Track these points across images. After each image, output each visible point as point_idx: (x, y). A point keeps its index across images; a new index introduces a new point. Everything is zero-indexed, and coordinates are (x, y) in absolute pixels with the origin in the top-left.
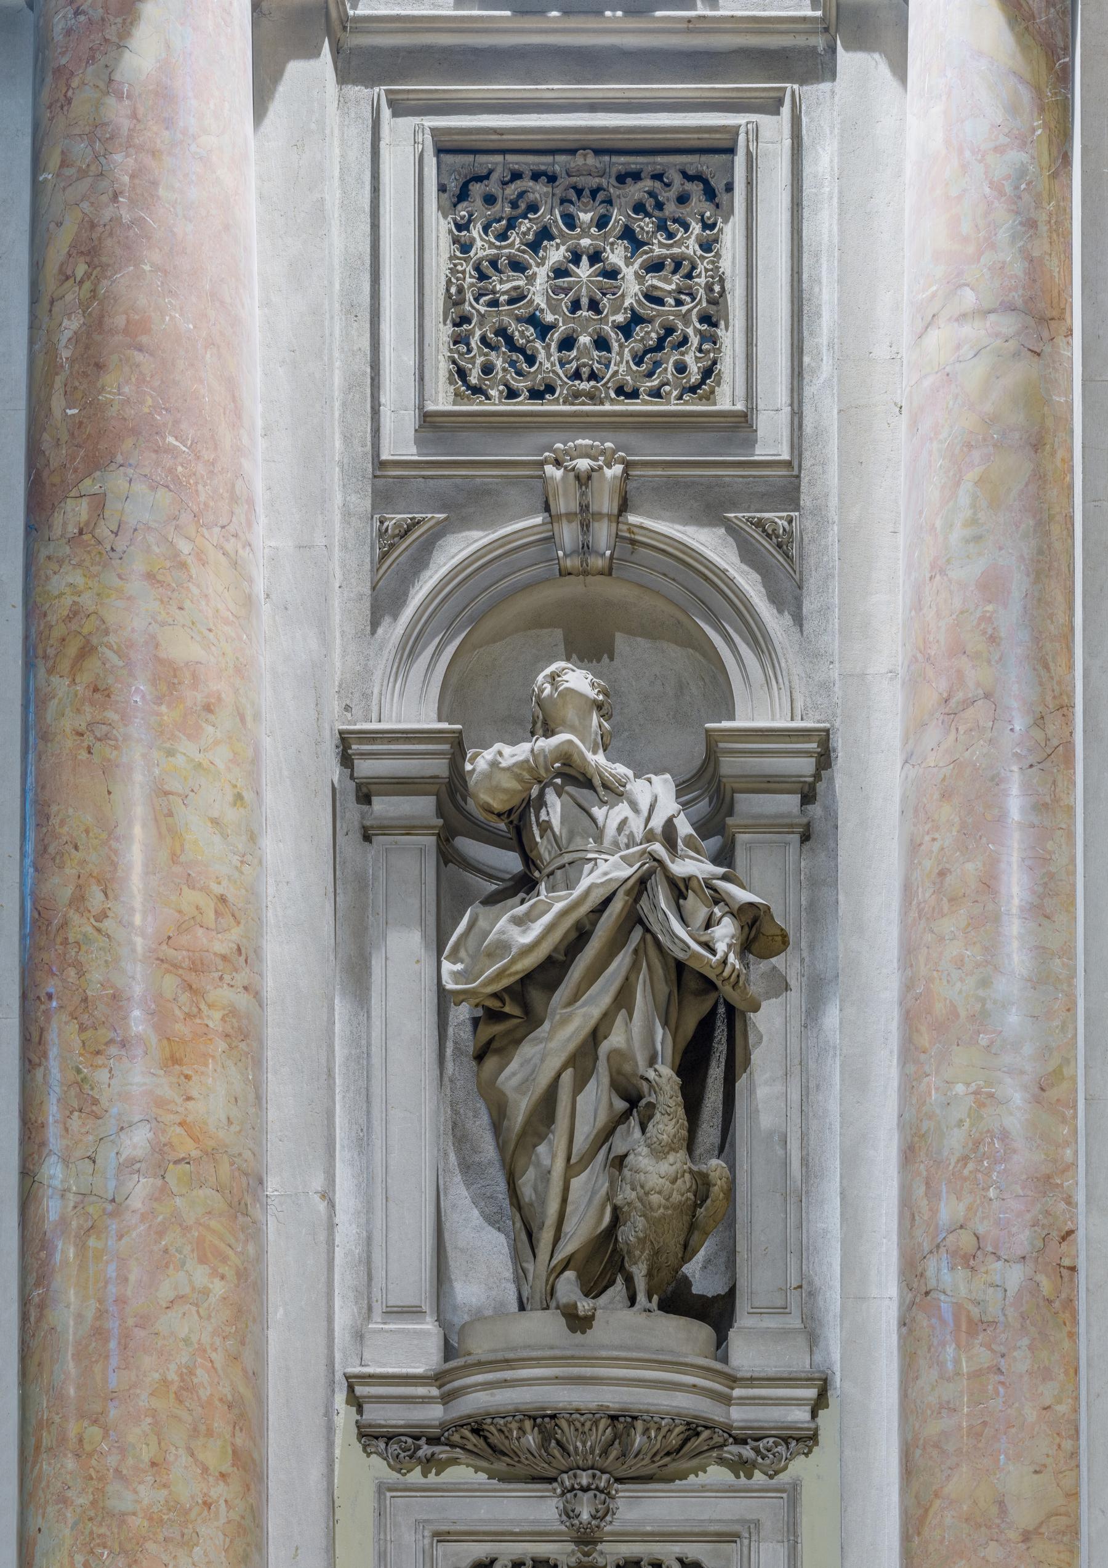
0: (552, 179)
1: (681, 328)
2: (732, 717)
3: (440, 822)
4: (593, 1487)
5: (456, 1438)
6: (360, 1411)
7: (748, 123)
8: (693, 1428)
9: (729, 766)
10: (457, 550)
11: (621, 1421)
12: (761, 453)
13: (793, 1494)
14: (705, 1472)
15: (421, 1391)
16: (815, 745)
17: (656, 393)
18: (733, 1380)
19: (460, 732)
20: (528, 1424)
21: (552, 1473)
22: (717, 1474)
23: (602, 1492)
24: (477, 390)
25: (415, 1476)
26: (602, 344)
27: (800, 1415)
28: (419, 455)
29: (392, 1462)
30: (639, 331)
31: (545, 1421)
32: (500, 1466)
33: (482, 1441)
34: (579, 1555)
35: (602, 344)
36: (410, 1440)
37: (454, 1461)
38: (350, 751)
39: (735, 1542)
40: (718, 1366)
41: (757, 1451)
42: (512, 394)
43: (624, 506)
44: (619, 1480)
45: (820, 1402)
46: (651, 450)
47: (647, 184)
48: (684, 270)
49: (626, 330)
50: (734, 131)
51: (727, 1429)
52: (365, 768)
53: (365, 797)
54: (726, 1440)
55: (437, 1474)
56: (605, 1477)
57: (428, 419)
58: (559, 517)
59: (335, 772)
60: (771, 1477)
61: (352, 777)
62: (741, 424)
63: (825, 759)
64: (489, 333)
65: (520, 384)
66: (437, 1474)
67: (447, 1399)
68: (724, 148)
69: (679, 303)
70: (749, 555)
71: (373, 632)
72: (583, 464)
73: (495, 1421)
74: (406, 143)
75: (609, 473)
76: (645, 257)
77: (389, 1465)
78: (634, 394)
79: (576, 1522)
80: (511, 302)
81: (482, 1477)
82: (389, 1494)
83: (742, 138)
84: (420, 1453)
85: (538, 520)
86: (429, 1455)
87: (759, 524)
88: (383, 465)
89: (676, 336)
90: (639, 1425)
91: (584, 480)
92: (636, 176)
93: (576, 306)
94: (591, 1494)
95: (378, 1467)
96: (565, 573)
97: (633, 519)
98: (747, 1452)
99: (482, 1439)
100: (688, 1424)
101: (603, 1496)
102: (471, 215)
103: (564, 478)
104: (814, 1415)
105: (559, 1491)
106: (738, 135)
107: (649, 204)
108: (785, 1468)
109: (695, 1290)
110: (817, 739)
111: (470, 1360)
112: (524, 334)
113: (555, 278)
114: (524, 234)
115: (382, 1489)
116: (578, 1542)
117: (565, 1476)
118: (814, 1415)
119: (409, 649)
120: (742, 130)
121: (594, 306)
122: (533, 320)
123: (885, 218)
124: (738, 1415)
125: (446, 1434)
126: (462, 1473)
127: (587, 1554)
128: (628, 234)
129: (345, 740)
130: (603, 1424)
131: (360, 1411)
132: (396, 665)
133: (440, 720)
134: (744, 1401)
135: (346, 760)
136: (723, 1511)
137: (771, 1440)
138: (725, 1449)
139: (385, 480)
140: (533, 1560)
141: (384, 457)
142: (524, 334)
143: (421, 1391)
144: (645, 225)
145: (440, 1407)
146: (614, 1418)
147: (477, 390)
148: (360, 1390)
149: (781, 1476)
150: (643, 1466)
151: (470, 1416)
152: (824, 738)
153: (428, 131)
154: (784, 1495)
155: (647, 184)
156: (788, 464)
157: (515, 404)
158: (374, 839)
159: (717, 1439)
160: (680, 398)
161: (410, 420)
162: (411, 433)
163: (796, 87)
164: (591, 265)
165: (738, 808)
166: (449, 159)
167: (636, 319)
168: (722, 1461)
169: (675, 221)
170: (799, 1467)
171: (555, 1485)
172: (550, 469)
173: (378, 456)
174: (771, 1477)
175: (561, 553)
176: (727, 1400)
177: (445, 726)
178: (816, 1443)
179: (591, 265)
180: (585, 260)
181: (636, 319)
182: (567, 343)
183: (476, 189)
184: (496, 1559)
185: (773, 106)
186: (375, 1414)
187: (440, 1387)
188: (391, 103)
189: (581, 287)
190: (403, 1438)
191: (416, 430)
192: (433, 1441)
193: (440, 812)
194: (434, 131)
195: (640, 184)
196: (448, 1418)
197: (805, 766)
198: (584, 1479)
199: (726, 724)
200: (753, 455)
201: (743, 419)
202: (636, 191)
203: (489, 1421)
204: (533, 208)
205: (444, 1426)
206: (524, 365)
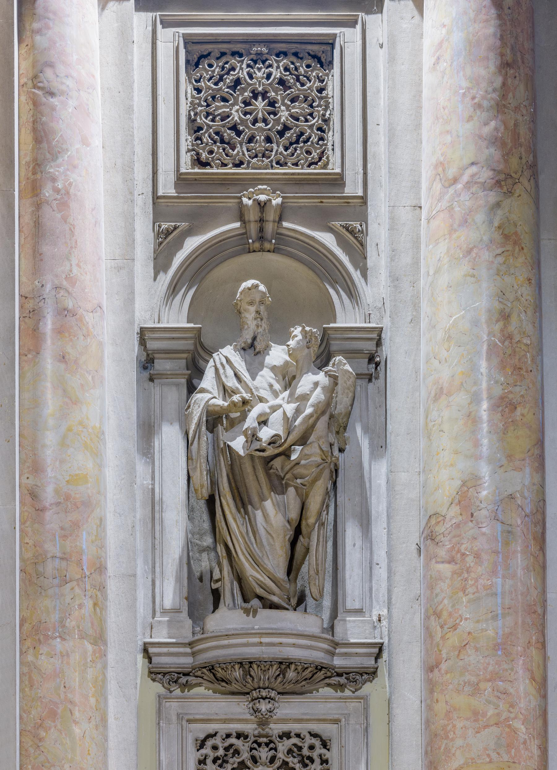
1: (305, 137)
2: (335, 322)
7: (341, 32)
8: (319, 668)
10: (192, 243)
11: (285, 664)
13: (365, 699)
15: (181, 650)
16: (376, 335)
17: (296, 164)
18: (337, 645)
19: (201, 328)
20: (237, 667)
21: (247, 690)
22: (328, 691)
30: (287, 135)
31: (247, 665)
32: (217, 686)
33: (212, 675)
35: (268, 140)
36: (176, 675)
37: (199, 685)
41: (347, 679)
42: (224, 165)
44: (279, 693)
45: (378, 656)
49: (281, 133)
50: (335, 35)
52: (152, 345)
55: (188, 691)
56: (274, 692)
60: (354, 692)
62: (338, 181)
63: (379, 343)
64: (211, 135)
65: (227, 160)
66: (188, 691)
67: (194, 654)
68: (329, 43)
70: (342, 242)
71: (155, 279)
73: (221, 665)
74: (169, 40)
77: (163, 686)
82: (164, 701)
83: (338, 39)
88: (158, 198)
93: (255, 121)
95: (158, 688)
97: (285, 224)
98: (342, 680)
99: (214, 674)
101: (273, 701)
104: (376, 662)
105: (250, 699)
106: (336, 37)
108: (361, 688)
111: (209, 635)
112: (228, 134)
113: (245, 107)
117: (254, 692)
118: (376, 662)
119: (173, 289)
120: (338, 35)
121: (265, 121)
122: (234, 128)
124: (338, 662)
125: (194, 671)
127: (263, 730)
129: (143, 331)
130: (275, 667)
133: (188, 322)
135: (142, 342)
137: (354, 674)
138: (332, 679)
142: (228, 134)
143: (181, 650)
146: (281, 663)
148: (151, 650)
149: (359, 691)
150: (289, 687)
151: (209, 663)
153: (181, 35)
154: (362, 701)
156: (362, 198)
157: (227, 169)
158: (155, 381)
159: (329, 674)
161: (172, 178)
163: (363, 14)
164: (263, 100)
167: (286, 128)
170: (367, 688)
173: (179, 171)
174: (354, 692)
175: (250, 241)
177: (192, 325)
179: (263, 100)
180: (260, 98)
181: (286, 128)
182: (251, 140)
185: (352, 24)
187: (191, 648)
188: (162, 22)
189: (258, 112)
190: (173, 674)
192: (186, 674)
197: (370, 346)
198: (264, 693)
199: (332, 325)
200: (343, 193)
203: (218, 665)
206: (230, 150)
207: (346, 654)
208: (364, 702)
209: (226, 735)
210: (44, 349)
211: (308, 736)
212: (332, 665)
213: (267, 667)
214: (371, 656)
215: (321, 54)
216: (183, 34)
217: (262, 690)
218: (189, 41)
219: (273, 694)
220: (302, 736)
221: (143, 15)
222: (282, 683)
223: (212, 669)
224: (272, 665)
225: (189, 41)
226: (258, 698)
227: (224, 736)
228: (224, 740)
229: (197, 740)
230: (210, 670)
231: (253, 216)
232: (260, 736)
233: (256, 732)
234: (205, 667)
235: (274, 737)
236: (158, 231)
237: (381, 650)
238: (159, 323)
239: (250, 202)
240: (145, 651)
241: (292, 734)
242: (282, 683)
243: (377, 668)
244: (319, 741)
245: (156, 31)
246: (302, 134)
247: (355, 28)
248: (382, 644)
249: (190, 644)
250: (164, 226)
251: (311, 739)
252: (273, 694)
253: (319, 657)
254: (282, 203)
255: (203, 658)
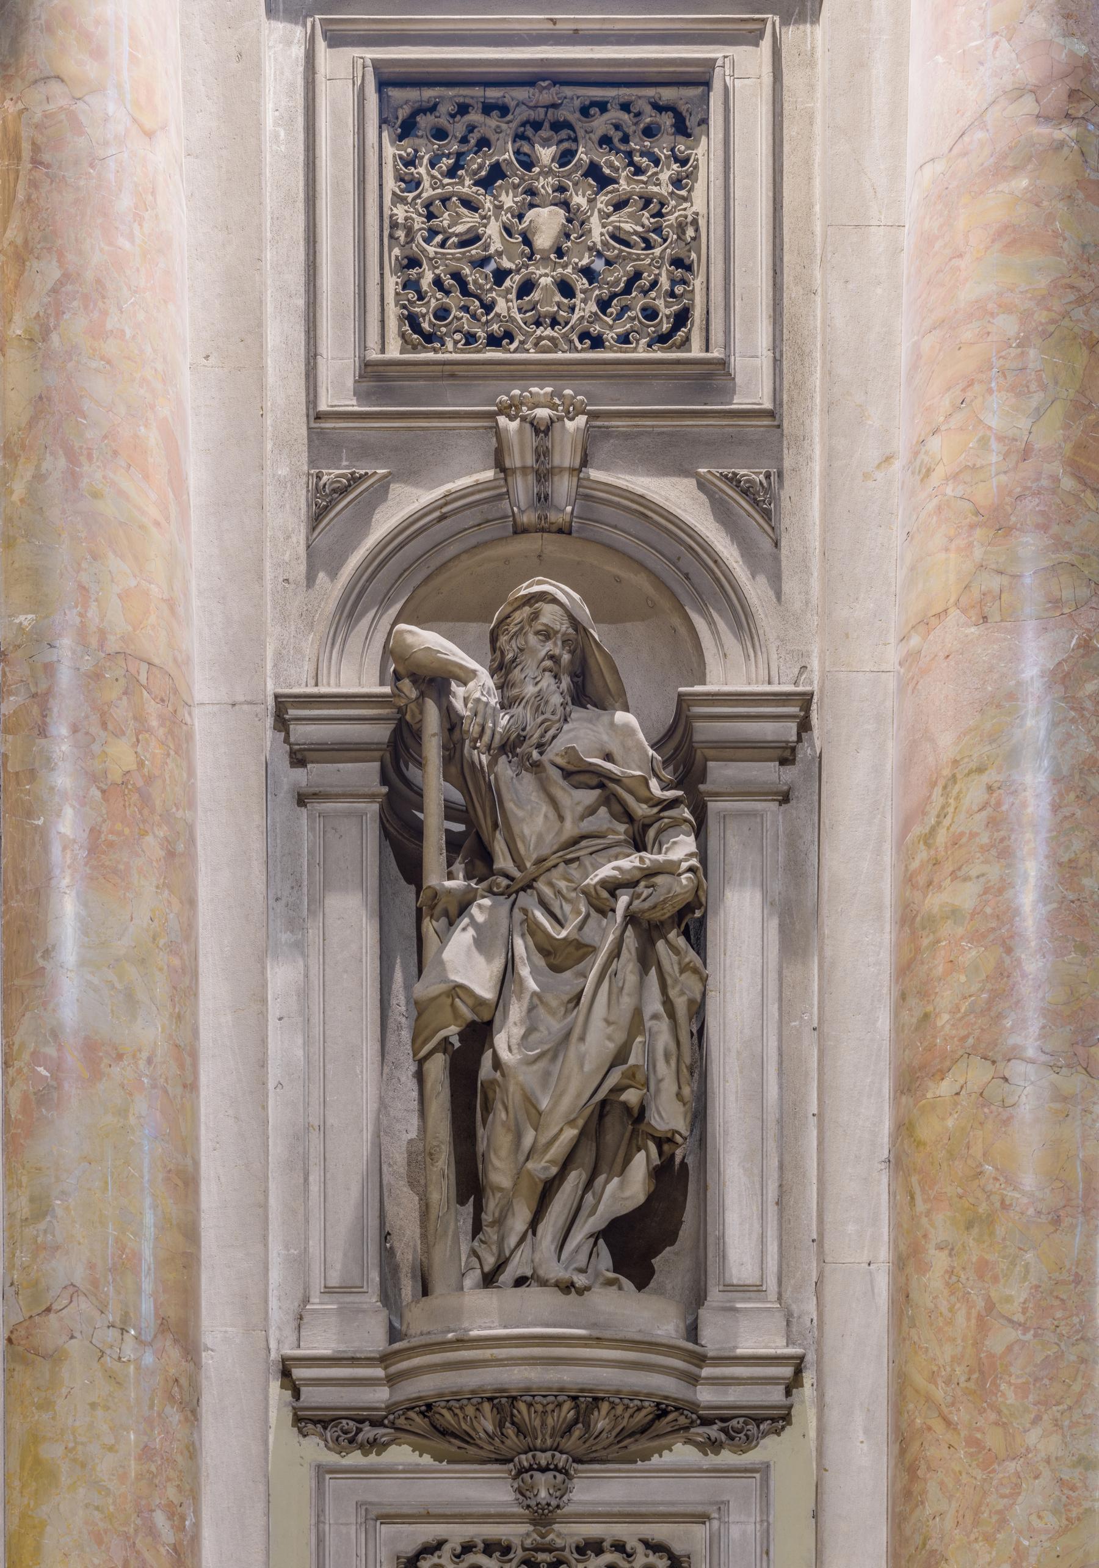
0: (504, 110)
3: (385, 790)
4: (552, 1467)
5: (401, 1422)
6: (297, 1394)
8: (661, 1412)
9: (704, 731)
10: (408, 502)
11: (585, 1403)
12: (739, 402)
14: (671, 1450)
16: (797, 709)
18: (701, 1359)
20: (487, 1407)
23: (560, 1472)
24: (429, 338)
25: (356, 1458)
26: (566, 288)
27: (775, 1395)
28: (359, 406)
29: (331, 1444)
31: (504, 1403)
32: (441, 1445)
34: (535, 1536)
38: (287, 717)
39: (704, 1523)
40: (690, 1346)
41: (723, 1430)
43: (584, 463)
44: (578, 1461)
46: (615, 402)
47: (615, 114)
48: (654, 207)
50: (711, 63)
51: (694, 1407)
52: (302, 733)
53: (299, 758)
54: (692, 1422)
57: (369, 369)
58: (514, 471)
59: (268, 734)
61: (286, 740)
62: (713, 376)
63: (805, 726)
67: (391, 1380)
68: (700, 79)
69: (649, 246)
70: (723, 513)
72: (543, 413)
74: (343, 71)
75: (570, 425)
76: (610, 196)
78: (597, 343)
79: (533, 1503)
80: (463, 244)
81: (427, 1460)
82: (328, 1476)
84: (360, 1437)
85: (490, 474)
86: (371, 1439)
87: (733, 480)
88: (319, 417)
89: (645, 282)
90: (605, 1407)
91: (542, 430)
92: (603, 107)
94: (550, 1474)
95: (315, 1449)
96: (519, 530)
98: (713, 1431)
100: (658, 1404)
102: (416, 151)
103: (520, 430)
104: (788, 1393)
107: (616, 136)
109: (653, 1261)
110: (800, 703)
111: (415, 1342)
114: (475, 173)
115: (322, 1471)
116: (534, 1522)
117: (523, 1457)
118: (788, 1393)
119: (350, 610)
123: (873, 163)
124: (705, 1396)
126: (401, 1454)
127: (543, 1536)
128: (593, 171)
129: (282, 703)
131: (297, 1394)
132: (334, 626)
134: (714, 1381)
135: (281, 722)
136: (688, 1493)
137: (742, 1420)
138: (692, 1430)
139: (322, 429)
140: (484, 1542)
141: (323, 407)
144: (610, 161)
145: (386, 1388)
147: (429, 338)
148: (298, 1373)
151: (420, 1398)
152: (806, 700)
153: (369, 63)
154: (758, 1475)
155: (615, 114)
156: (771, 414)
159: (682, 1420)
160: (649, 346)
162: (350, 383)
165: (710, 777)
166: (395, 93)
168: (689, 1441)
169: (642, 154)
170: (769, 1449)
171: (511, 1466)
172: (502, 420)
176: (694, 1380)
178: (790, 1423)
183: (425, 122)
184: (446, 1541)
185: (754, 38)
186: (312, 1396)
187: (385, 1368)
191: (355, 381)
192: (376, 1423)
193: (384, 780)
194: (377, 64)
195: (606, 116)
196: (394, 1399)
198: (543, 1458)
199: (698, 688)
201: (721, 367)
202: (601, 124)
203: (443, 1404)
204: (484, 143)
205: (390, 1408)
207: (714, 1381)
208: (761, 1479)
209: (463, 1547)
210: (1019, 92)
211: (640, 1549)
212: (693, 1403)
213: (550, 1407)
214: (778, 1384)
215: (675, 106)
216: (372, 60)
217: (538, 1454)
218: (388, 80)
219: (562, 1459)
220: (628, 1548)
221: (280, 27)
222: (583, 1440)
223: (428, 1409)
224: (560, 1405)
225: (388, 80)
226: (531, 1468)
227: (459, 1550)
228: (458, 1557)
229: (398, 1558)
230: (421, 1413)
231: (519, 456)
232: (538, 1549)
233: (528, 1543)
234: (413, 1408)
235: (567, 1549)
236: (317, 484)
237: (798, 1372)
238: (316, 685)
239: (514, 425)
240: (286, 1373)
241: (606, 1545)
242: (583, 1440)
243: (790, 1407)
244: (665, 1559)
245: (314, 56)
246: (638, 275)
247: (757, 45)
248: (802, 1358)
249: (384, 1359)
250: (330, 474)
251: (647, 1556)
252: (562, 1459)
253: (667, 1386)
254: (588, 427)
255: (413, 1389)
